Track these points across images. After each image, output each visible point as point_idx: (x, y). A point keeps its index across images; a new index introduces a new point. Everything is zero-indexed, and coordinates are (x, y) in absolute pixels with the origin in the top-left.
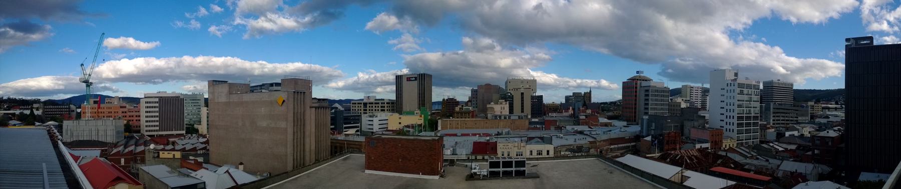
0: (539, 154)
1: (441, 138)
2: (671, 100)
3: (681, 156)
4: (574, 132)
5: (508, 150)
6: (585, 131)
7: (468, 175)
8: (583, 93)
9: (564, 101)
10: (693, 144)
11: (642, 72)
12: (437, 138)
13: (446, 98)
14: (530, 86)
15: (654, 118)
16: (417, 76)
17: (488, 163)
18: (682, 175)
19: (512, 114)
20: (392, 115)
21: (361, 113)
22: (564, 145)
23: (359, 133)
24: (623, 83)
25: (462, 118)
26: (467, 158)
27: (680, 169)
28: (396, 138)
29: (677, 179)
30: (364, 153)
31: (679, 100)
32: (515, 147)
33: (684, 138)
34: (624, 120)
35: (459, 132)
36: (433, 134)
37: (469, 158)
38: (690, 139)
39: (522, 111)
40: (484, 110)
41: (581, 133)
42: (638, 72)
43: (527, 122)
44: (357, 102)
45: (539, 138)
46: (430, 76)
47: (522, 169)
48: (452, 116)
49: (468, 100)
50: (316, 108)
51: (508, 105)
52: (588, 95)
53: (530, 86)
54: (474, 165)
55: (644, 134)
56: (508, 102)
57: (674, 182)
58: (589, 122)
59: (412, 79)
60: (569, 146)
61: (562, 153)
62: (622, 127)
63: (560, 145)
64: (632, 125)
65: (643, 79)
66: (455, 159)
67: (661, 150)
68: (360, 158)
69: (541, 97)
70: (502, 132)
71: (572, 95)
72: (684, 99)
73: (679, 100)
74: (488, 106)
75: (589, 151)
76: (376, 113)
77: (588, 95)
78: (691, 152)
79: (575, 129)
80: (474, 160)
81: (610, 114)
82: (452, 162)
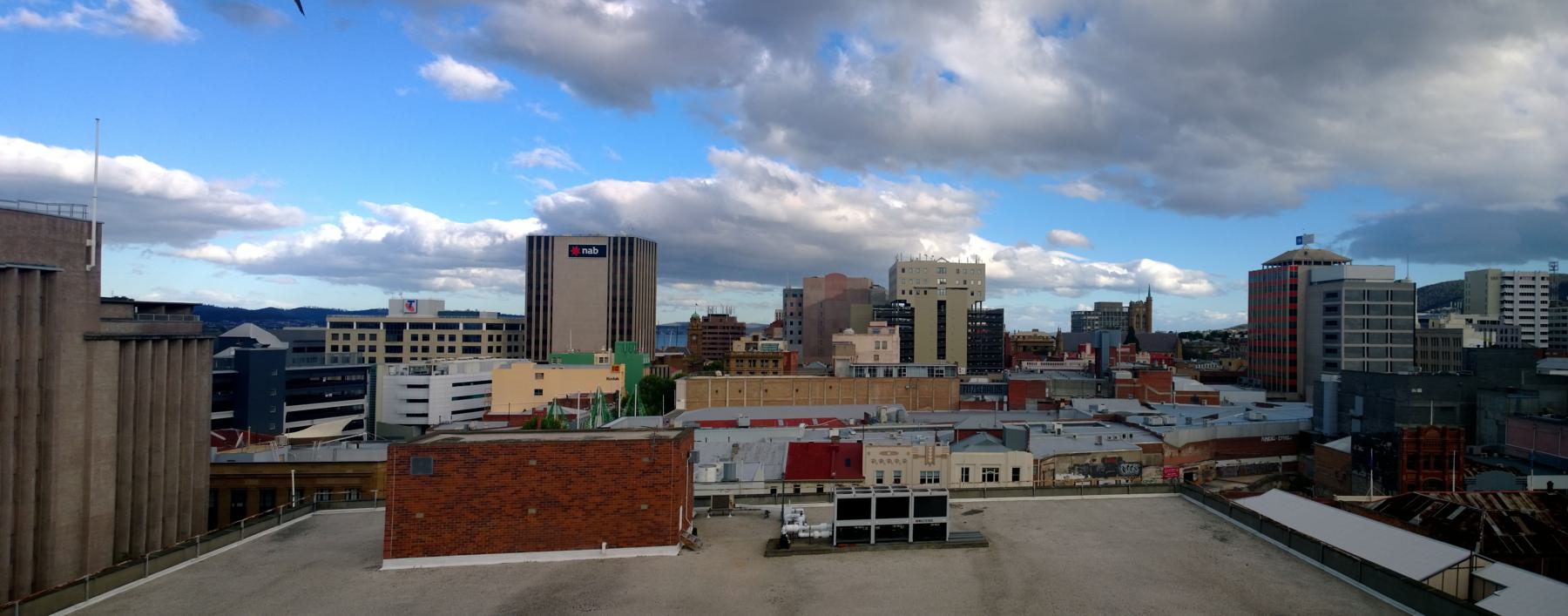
0: (990, 478)
1: (687, 433)
2: (1423, 321)
3: (1467, 512)
4: (1095, 417)
5: (897, 468)
6: (1130, 414)
7: (771, 540)
8: (1126, 304)
9: (1067, 328)
10: (1518, 473)
11: (1310, 239)
12: (673, 434)
13: (702, 314)
14: (965, 282)
15: (1354, 383)
16: (606, 243)
17: (834, 505)
18: (1472, 578)
19: (908, 361)
20: (508, 366)
21: (372, 360)
22: (1067, 455)
23: (363, 432)
24: (1252, 274)
25: (752, 373)
26: (768, 492)
27: (1465, 553)
28: (519, 441)
29: (1454, 585)
30: (380, 502)
31: (1455, 321)
32: (916, 456)
33: (1477, 449)
34: (1257, 387)
35: (743, 415)
36: (657, 421)
37: (773, 491)
38: (1501, 456)
39: (941, 354)
40: (823, 351)
41: (1117, 419)
42: (1299, 240)
43: (955, 386)
44: (355, 320)
45: (989, 431)
46: (651, 246)
47: (937, 520)
48: (721, 369)
49: (772, 319)
50: (123, 341)
51: (897, 337)
52: (1143, 311)
53: (965, 282)
54: (789, 509)
55: (1327, 429)
56: (897, 327)
57: (1440, 595)
58: (1143, 388)
59: (590, 252)
60: (1081, 458)
61: (1059, 477)
62: (1250, 407)
63: (1052, 454)
64: (1284, 400)
65: (1317, 258)
66: (731, 493)
67: (1386, 485)
68: (369, 521)
69: (998, 314)
70: (879, 415)
71: (1091, 309)
72: (1476, 318)
73: (1455, 321)
74: (836, 338)
75: (1141, 472)
76: (440, 361)
77: (1143, 311)
78: (1506, 501)
79: (1101, 408)
80: (789, 495)
81: (1211, 366)
82: (721, 505)
